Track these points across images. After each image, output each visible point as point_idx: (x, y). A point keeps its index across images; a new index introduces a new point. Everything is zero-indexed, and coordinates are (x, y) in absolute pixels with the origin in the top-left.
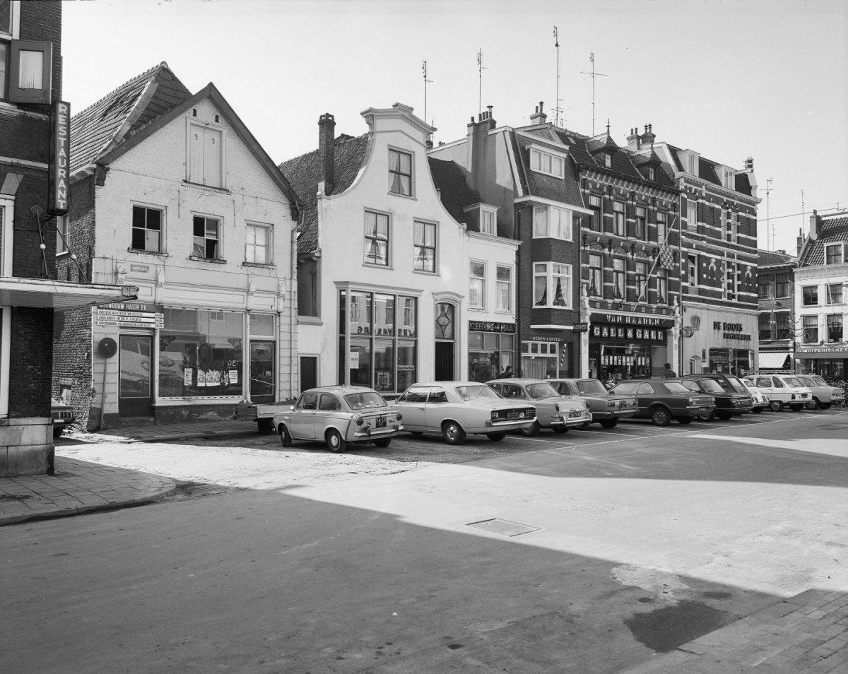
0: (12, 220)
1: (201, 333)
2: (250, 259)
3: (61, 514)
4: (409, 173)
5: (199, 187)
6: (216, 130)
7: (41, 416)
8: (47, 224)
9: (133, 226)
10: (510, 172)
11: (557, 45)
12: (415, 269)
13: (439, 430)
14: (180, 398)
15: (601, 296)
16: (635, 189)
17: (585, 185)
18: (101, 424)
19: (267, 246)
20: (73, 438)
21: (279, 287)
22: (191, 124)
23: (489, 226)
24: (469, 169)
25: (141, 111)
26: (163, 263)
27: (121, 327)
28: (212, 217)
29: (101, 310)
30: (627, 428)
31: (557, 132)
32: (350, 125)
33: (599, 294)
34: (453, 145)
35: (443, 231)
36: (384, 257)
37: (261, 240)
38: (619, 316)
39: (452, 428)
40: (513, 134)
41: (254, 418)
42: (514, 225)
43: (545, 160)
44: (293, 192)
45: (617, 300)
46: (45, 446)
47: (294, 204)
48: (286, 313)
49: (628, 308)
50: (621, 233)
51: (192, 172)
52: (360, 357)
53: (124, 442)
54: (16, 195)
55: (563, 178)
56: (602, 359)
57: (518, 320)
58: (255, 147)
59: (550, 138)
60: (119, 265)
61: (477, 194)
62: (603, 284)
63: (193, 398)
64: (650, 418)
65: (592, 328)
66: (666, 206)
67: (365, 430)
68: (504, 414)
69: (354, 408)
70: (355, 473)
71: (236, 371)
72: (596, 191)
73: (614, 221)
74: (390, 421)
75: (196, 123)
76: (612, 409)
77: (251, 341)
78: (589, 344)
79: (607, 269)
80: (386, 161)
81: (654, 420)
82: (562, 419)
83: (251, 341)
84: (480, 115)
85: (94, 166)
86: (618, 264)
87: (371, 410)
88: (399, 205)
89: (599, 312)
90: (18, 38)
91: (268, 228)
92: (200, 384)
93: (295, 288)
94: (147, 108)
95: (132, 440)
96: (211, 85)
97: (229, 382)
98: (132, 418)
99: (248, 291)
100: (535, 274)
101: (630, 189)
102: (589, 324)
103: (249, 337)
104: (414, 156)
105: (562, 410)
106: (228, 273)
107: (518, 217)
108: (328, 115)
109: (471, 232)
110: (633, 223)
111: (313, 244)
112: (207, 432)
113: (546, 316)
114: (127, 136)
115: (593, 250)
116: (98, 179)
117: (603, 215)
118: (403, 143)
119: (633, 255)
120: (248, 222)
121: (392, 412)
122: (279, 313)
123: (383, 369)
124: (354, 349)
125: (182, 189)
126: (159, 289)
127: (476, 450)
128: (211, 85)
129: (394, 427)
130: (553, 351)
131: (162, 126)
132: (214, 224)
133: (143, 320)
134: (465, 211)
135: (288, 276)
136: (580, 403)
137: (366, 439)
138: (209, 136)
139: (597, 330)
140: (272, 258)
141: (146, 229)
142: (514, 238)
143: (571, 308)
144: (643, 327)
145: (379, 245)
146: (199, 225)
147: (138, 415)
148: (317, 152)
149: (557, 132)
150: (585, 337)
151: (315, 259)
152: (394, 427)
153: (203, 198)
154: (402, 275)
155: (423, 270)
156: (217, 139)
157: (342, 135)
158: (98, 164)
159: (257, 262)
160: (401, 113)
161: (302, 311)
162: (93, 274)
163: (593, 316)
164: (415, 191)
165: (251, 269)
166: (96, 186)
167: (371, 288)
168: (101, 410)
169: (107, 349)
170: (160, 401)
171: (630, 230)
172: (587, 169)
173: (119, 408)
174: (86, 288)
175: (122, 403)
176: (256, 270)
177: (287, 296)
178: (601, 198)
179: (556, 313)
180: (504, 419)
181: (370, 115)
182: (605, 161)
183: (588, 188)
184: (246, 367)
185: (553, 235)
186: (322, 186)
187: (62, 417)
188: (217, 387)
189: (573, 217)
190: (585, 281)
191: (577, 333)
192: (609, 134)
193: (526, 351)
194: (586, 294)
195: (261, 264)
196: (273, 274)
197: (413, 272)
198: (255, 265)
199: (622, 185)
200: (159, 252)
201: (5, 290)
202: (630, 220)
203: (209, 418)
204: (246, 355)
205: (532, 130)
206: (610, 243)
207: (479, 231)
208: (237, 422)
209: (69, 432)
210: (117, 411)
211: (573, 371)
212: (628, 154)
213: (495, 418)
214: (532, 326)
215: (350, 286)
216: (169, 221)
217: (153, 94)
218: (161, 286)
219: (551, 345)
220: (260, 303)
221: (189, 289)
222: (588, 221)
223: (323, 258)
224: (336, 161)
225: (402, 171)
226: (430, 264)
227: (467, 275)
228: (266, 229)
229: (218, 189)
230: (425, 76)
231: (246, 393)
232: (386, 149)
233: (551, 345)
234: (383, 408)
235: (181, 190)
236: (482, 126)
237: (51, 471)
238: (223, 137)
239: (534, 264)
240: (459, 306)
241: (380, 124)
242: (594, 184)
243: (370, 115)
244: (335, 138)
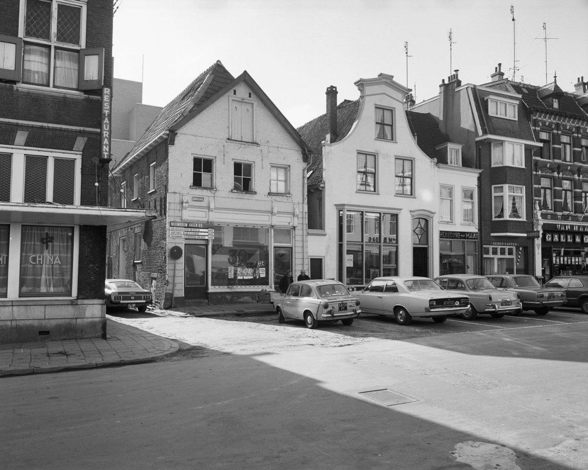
0: (81, 167)
1: (260, 243)
2: (274, 190)
3: (84, 367)
4: (391, 124)
5: (237, 142)
6: (250, 103)
7: (98, 299)
8: (102, 170)
9: (235, 175)
10: (472, 118)
11: (513, 20)
12: (396, 194)
13: (392, 314)
14: (226, 287)
15: (551, 210)
16: (580, 124)
17: (535, 123)
18: (172, 304)
19: (286, 181)
20: (153, 313)
21: (294, 209)
22: (233, 100)
23: (455, 160)
24: (441, 118)
25: (201, 94)
26: (213, 195)
27: (186, 239)
28: (247, 162)
29: (172, 228)
30: (561, 315)
31: (512, 85)
32: (348, 93)
33: (550, 208)
34: (430, 101)
35: (418, 165)
36: (372, 184)
37: (282, 177)
38: (568, 225)
39: (401, 312)
40: (474, 89)
41: (268, 302)
42: (477, 157)
43: (501, 108)
44: (304, 142)
45: (566, 213)
46: (100, 319)
47: (305, 150)
48: (299, 227)
49: (575, 219)
50: (568, 159)
52: (354, 258)
53: (183, 317)
54: (83, 151)
55: (516, 119)
56: (554, 259)
57: (480, 229)
58: (276, 112)
59: (507, 90)
60: (184, 197)
61: (448, 136)
62: (553, 200)
63: (235, 287)
64: (579, 307)
65: (544, 235)
66: (570, 130)
67: (330, 312)
68: (440, 302)
69: (323, 295)
70: (312, 345)
71: (264, 268)
72: (545, 127)
73: (562, 150)
74: (350, 306)
75: (236, 99)
76: (541, 299)
77: (274, 247)
78: (542, 248)
79: (557, 188)
80: (373, 116)
81: (583, 309)
82: (494, 307)
84: (449, 77)
85: (168, 132)
86: (567, 184)
87: (336, 297)
88: (383, 148)
89: (550, 223)
90: (85, 48)
91: (287, 168)
92: (239, 278)
93: (306, 210)
94: (206, 92)
95: (189, 315)
96: (245, 72)
97: (260, 276)
98: (193, 300)
99: (272, 213)
100: (494, 194)
101: (576, 124)
102: (541, 232)
103: (273, 244)
104: (395, 111)
105: (494, 300)
106: (259, 200)
107: (479, 151)
108: (332, 87)
109: (440, 164)
110: (578, 151)
111: (320, 179)
112: (238, 311)
113: (504, 226)
114: (190, 111)
115: (544, 174)
116: (170, 140)
117: (552, 146)
118: (386, 102)
119: (579, 176)
120: (273, 165)
121: (352, 299)
122: (294, 227)
123: (364, 267)
124: (349, 252)
125: (226, 144)
126: (211, 213)
127: (417, 330)
128: (245, 72)
129: (353, 311)
130: (510, 253)
131: (212, 102)
132: (249, 167)
133: (200, 234)
134: (437, 149)
135: (301, 201)
136: (512, 295)
137: (331, 319)
138: (244, 107)
139: (549, 237)
141: (202, 172)
142: (476, 168)
143: (525, 220)
144: (560, 232)
145: (369, 177)
146: (238, 167)
147: (197, 299)
148: (325, 115)
149: (512, 85)
150: (538, 242)
151: (321, 189)
152: (353, 311)
153: (240, 149)
154: (387, 197)
155: (403, 194)
156: (250, 110)
157: (345, 100)
158: (170, 131)
159: (279, 192)
160: (384, 80)
161: (311, 225)
162: (167, 204)
163: (544, 226)
164: (396, 137)
165: (274, 198)
167: (380, 210)
168: (172, 294)
169: (176, 253)
170: (212, 289)
171: (576, 156)
172: (537, 111)
173: (185, 294)
174: (121, 211)
175: (187, 290)
176: (278, 198)
177: (300, 216)
178: (550, 133)
180: (442, 306)
181: (361, 84)
182: (553, 104)
183: (538, 126)
184: (271, 266)
185: (508, 163)
186: (328, 137)
187: (144, 299)
188: (249, 280)
189: (525, 149)
190: (537, 198)
191: (531, 239)
192: (556, 83)
193: (488, 253)
194: (538, 208)
195: (281, 194)
196: (290, 200)
197: (395, 196)
198: (277, 194)
199: (568, 122)
200: (211, 188)
201: (77, 215)
202: (576, 149)
203: (245, 301)
204: (271, 258)
205: (492, 85)
206: (559, 168)
207: (447, 163)
208: (260, 304)
209: (153, 309)
210: (183, 295)
211: (528, 268)
212: (574, 97)
213: (433, 305)
214: (492, 234)
215: (346, 207)
216: (217, 166)
217: (210, 82)
218: (212, 211)
219: (501, 249)
220: (281, 221)
221: (231, 212)
222: (540, 152)
223: (326, 188)
224: (338, 119)
225: (386, 122)
226: (408, 188)
227: (443, 196)
228: (285, 169)
229: (250, 143)
230: (407, 53)
231: (271, 284)
233: (501, 249)
234: (346, 296)
236: (451, 86)
237: (104, 337)
238: (254, 107)
240: (431, 220)
241: (368, 90)
242: (544, 123)
243: (361, 84)
244: (338, 103)
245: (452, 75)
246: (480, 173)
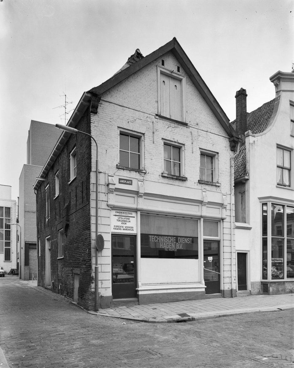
9: (120, 149)
48: (228, 219)
51: (162, 110)
125: (155, 120)
138: (170, 83)
140: (217, 178)
166: (91, 114)
232: (198, 153)
235: (154, 122)
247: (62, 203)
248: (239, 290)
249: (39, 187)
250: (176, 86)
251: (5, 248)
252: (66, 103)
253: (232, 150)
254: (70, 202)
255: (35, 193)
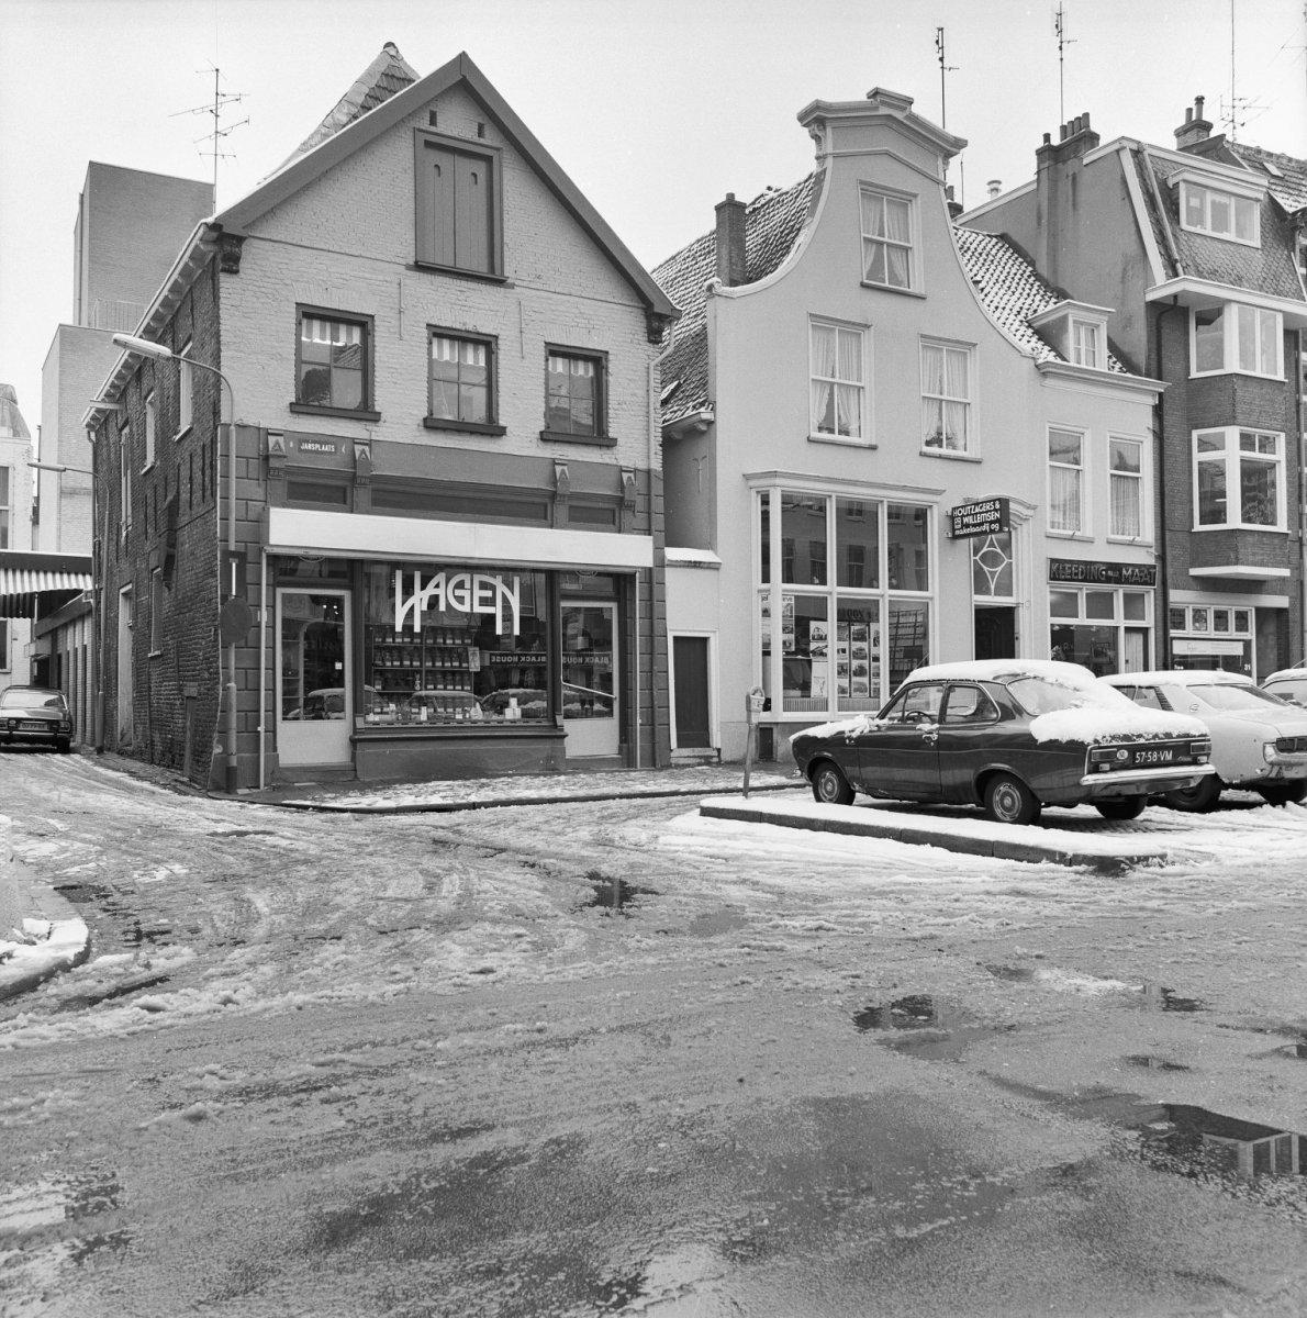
83: (825, 620)
143: (1285, 530)
156: (482, 177)
179: (1250, 539)
193: (1181, 625)
214: (1194, 572)
223: (719, 424)
230: (941, 59)
239: (1195, 434)
245: (1065, 123)
246: (1160, 394)
247: (161, 490)
248: (679, 746)
249: (100, 424)
250: (475, 175)
251: (343, 686)
252: (221, 99)
253: (650, 341)
254: (178, 492)
255: (90, 439)
